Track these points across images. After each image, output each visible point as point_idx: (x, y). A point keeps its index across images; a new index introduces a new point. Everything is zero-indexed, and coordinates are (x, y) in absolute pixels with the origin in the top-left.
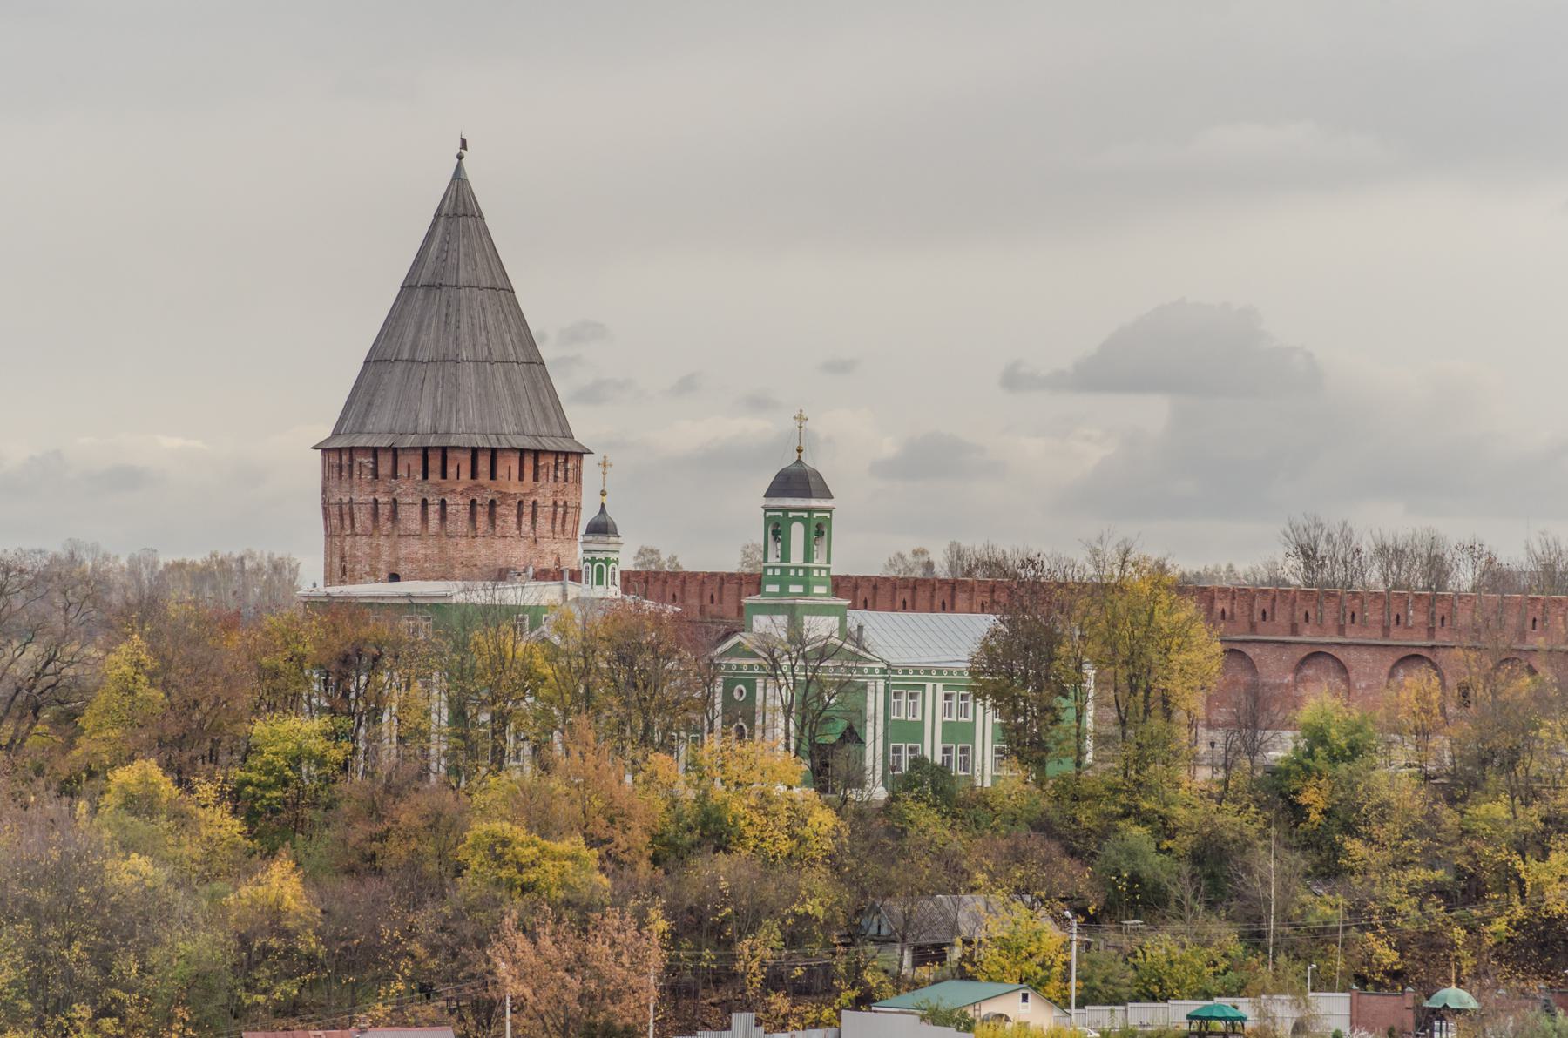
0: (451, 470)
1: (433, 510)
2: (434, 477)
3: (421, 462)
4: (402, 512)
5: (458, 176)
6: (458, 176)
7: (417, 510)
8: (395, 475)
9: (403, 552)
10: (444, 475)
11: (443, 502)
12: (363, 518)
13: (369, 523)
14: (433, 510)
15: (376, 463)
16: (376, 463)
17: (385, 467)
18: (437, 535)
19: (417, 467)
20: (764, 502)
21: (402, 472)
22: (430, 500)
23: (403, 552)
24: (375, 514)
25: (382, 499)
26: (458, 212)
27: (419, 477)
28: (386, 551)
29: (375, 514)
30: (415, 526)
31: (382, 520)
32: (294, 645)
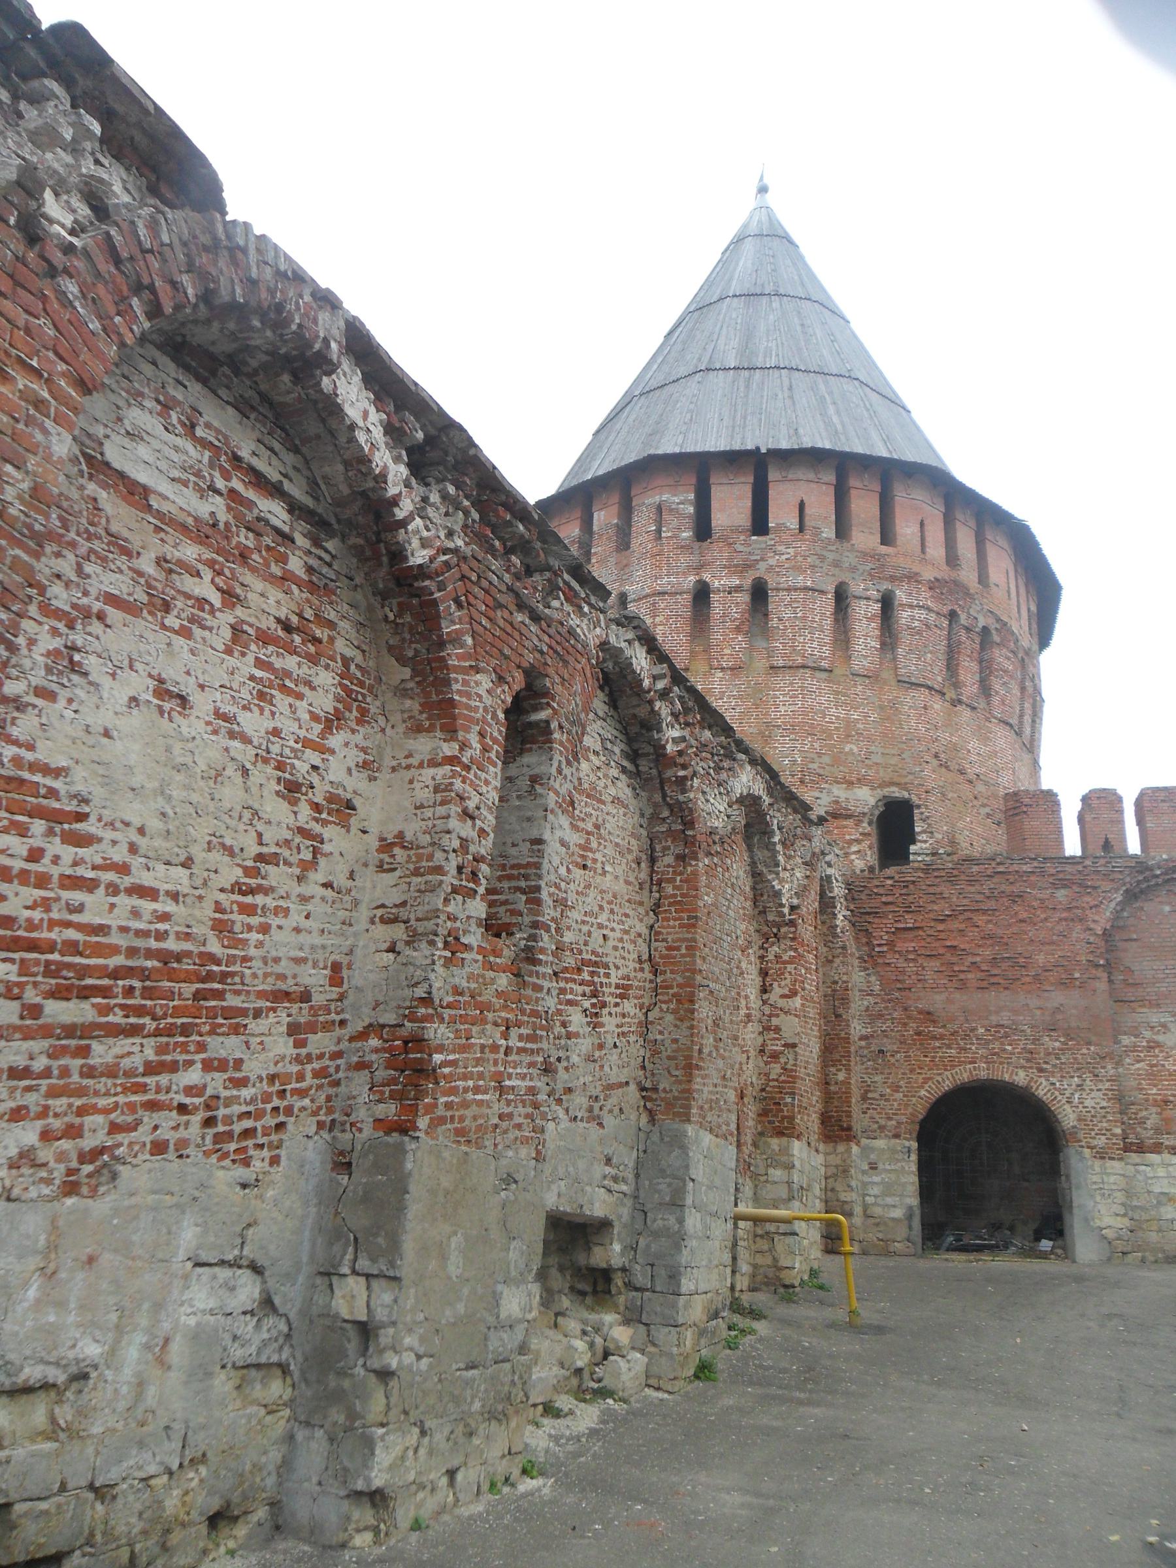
0: (906, 530)
1: (865, 613)
2: (865, 537)
4: (781, 608)
8: (760, 525)
10: (887, 537)
11: (887, 602)
14: (865, 613)
17: (731, 504)
18: (871, 677)
19: (821, 506)
21: (781, 514)
22: (857, 587)
25: (718, 581)
27: (829, 532)
30: (817, 644)
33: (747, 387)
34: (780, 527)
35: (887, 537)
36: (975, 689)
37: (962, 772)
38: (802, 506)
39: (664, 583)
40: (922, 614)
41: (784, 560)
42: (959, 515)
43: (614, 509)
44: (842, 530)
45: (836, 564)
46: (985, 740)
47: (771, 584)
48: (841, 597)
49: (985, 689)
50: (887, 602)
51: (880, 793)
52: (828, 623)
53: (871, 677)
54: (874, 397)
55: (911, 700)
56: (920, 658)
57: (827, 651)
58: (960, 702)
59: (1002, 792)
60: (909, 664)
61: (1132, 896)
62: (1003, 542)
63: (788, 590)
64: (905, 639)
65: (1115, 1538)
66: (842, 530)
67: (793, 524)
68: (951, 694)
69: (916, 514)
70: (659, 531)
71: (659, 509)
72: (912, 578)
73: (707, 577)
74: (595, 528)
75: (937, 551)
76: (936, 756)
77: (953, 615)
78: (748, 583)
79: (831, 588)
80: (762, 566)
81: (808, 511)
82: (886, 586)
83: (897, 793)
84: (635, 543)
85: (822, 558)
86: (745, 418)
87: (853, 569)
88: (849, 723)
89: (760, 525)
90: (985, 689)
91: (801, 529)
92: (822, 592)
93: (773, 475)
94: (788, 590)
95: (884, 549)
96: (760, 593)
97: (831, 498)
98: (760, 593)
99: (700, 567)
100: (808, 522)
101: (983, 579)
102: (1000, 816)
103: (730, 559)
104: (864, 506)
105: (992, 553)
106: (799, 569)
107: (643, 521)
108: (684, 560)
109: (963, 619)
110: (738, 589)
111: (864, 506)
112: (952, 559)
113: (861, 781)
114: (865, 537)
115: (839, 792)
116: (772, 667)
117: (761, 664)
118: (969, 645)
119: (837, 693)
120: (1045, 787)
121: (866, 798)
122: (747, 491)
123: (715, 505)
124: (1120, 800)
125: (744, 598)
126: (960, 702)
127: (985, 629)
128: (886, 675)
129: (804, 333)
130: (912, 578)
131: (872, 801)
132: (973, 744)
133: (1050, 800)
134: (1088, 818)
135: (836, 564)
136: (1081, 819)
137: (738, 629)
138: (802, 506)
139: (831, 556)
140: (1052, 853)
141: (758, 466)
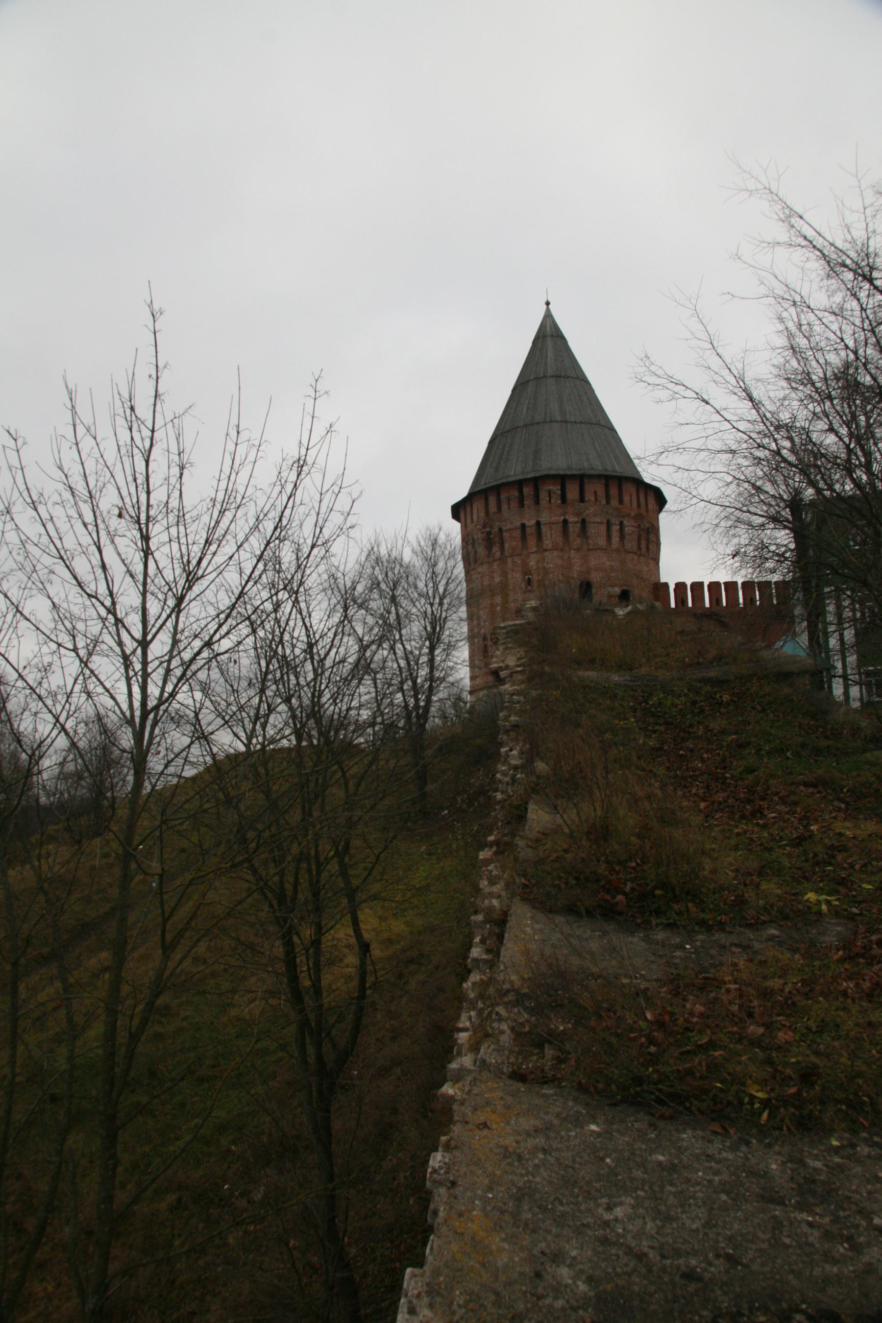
0: (626, 499)
1: (615, 528)
2: (614, 503)
3: (604, 489)
4: (592, 530)
5: (548, 316)
6: (548, 316)
7: (603, 528)
8: (582, 499)
9: (593, 563)
10: (621, 502)
11: (621, 524)
12: (551, 537)
13: (560, 540)
14: (615, 528)
15: (563, 490)
16: (563, 490)
17: (573, 492)
18: (617, 550)
19: (601, 493)
20: (722, 581)
21: (589, 496)
22: (613, 521)
23: (593, 563)
24: (524, 537)
25: (571, 519)
26: (549, 342)
27: (604, 502)
28: (577, 562)
29: (524, 537)
30: (602, 541)
31: (572, 537)
32: (274, 687)
34: (589, 501)
35: (621, 502)
38: (595, 492)
39: (553, 519)
40: (632, 529)
41: (590, 510)
48: (609, 525)
49: (648, 548)
52: (605, 534)
56: (631, 545)
64: (627, 537)
65: (226, 1187)
66: (608, 498)
67: (593, 499)
72: (628, 515)
73: (567, 517)
75: (635, 505)
77: (639, 526)
78: (580, 520)
79: (605, 522)
80: (585, 514)
82: (621, 519)
83: (625, 588)
84: (542, 503)
88: (612, 567)
89: (582, 499)
90: (648, 548)
93: (586, 481)
95: (620, 506)
96: (583, 522)
98: (583, 522)
99: (565, 513)
101: (647, 511)
104: (614, 492)
105: (649, 498)
106: (595, 516)
107: (543, 495)
109: (642, 527)
110: (577, 522)
111: (614, 492)
112: (639, 506)
113: (616, 585)
114: (614, 503)
120: (663, 580)
125: (579, 525)
130: (628, 515)
132: (645, 569)
133: (666, 585)
135: (607, 513)
136: (675, 590)
137: (578, 536)
138: (595, 492)
141: (582, 479)
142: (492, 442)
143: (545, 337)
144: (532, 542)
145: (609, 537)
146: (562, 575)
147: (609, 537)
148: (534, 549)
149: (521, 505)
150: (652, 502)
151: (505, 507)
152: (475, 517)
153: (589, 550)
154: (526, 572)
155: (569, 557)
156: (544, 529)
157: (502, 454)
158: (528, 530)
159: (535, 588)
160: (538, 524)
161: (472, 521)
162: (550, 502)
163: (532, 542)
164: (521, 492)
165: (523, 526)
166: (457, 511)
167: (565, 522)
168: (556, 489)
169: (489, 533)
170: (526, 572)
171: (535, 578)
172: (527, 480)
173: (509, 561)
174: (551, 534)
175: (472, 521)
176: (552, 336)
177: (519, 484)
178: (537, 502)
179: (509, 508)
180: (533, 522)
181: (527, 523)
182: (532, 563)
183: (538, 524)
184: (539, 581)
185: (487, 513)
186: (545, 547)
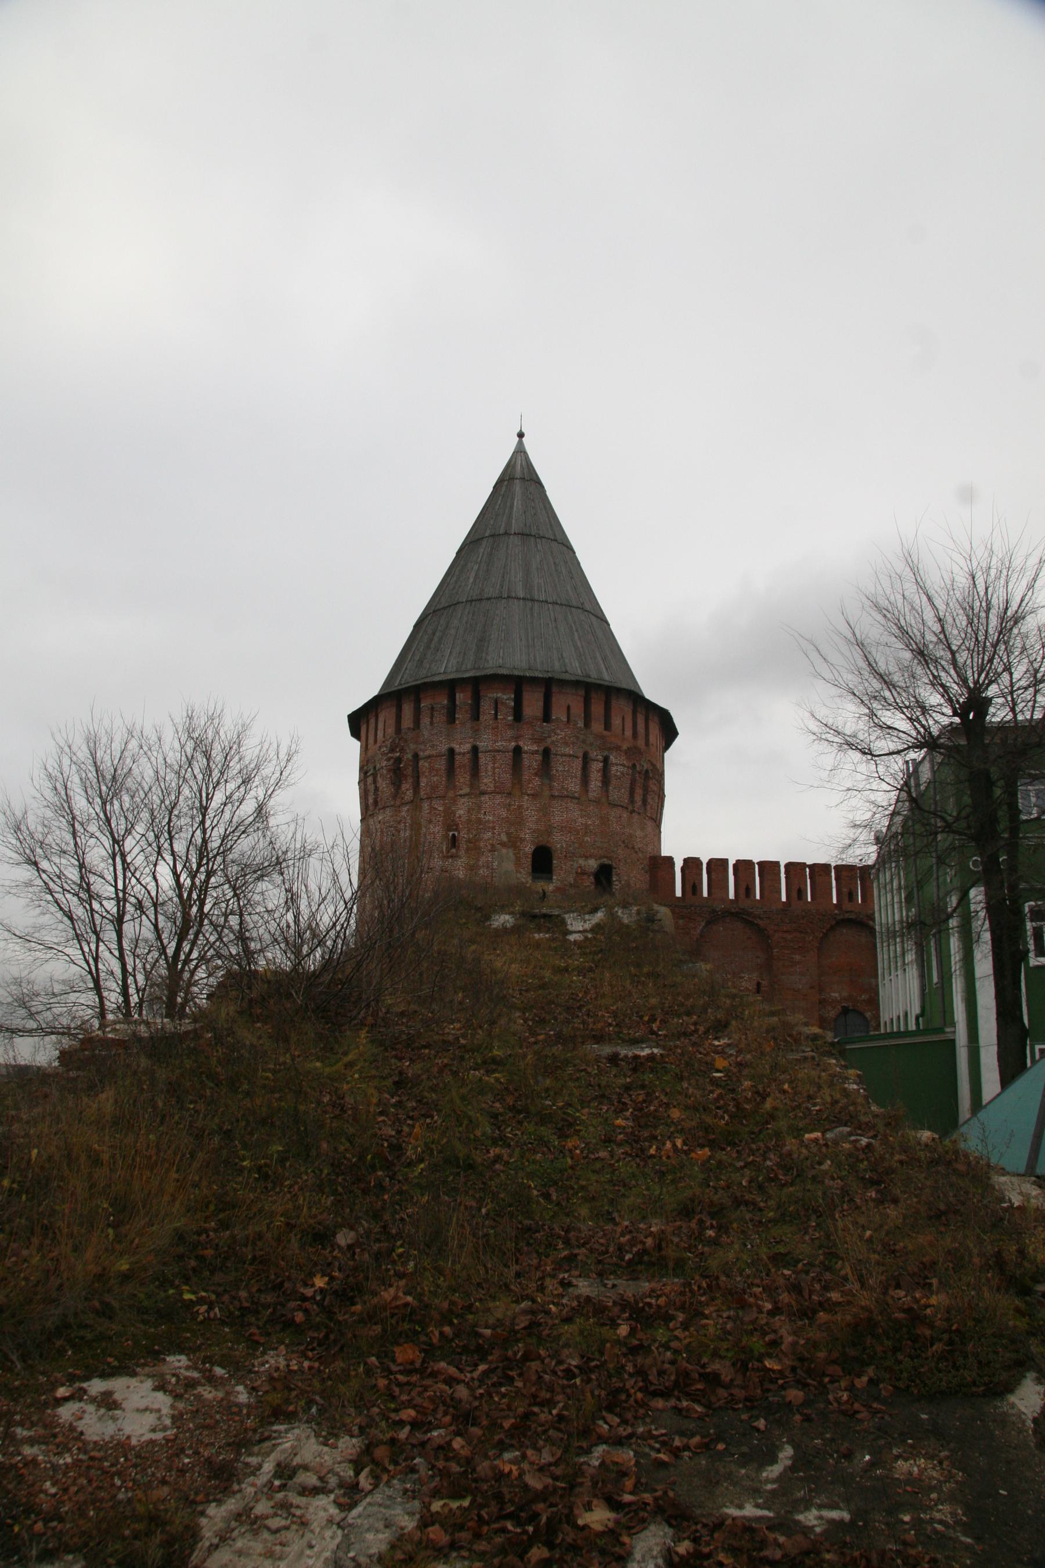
0: (616, 721)
1: (596, 766)
2: (597, 727)
4: (558, 766)
6: (520, 451)
7: (578, 764)
8: (547, 717)
10: (607, 726)
11: (606, 760)
12: (494, 771)
13: (507, 777)
14: (596, 766)
17: (533, 705)
18: (597, 802)
19: (578, 710)
21: (558, 713)
22: (593, 754)
23: (558, 817)
25: (527, 747)
27: (581, 724)
30: (574, 786)
33: (532, 615)
34: (557, 719)
35: (607, 726)
36: (640, 803)
37: (633, 848)
38: (569, 708)
42: (639, 709)
43: (469, 694)
44: (587, 724)
45: (584, 742)
46: (643, 829)
47: (553, 750)
49: (645, 802)
50: (606, 760)
51: (599, 862)
53: (597, 802)
54: (593, 619)
55: (614, 813)
56: (618, 793)
57: (578, 788)
58: (634, 811)
59: (648, 855)
60: (614, 795)
61: (708, 923)
62: (656, 719)
63: (562, 755)
64: (614, 782)
66: (587, 724)
68: (630, 808)
69: (621, 709)
70: (496, 714)
71: (496, 702)
72: (618, 748)
73: (521, 744)
74: (457, 703)
75: (628, 733)
76: (624, 842)
77: (634, 765)
78: (542, 748)
79: (581, 755)
80: (549, 740)
81: (572, 712)
82: (606, 753)
83: (606, 861)
85: (577, 738)
86: (533, 640)
87: (591, 744)
88: (587, 826)
89: (547, 717)
90: (645, 802)
91: (568, 721)
92: (577, 757)
93: (554, 689)
94: (562, 755)
95: (606, 733)
96: (546, 753)
97: (582, 705)
98: (546, 753)
99: (517, 738)
100: (572, 718)
101: (647, 744)
102: (647, 868)
103: (533, 735)
106: (566, 744)
107: (486, 706)
108: (510, 733)
109: (638, 768)
110: (536, 752)
112: (635, 735)
113: (591, 856)
114: (597, 727)
115: (582, 862)
116: (552, 796)
117: (547, 793)
118: (640, 781)
119: (581, 810)
121: (593, 864)
122: (541, 696)
123: (525, 703)
124: (702, 864)
125: (539, 757)
126: (634, 811)
127: (647, 771)
128: (604, 800)
129: (556, 571)
130: (618, 748)
131: (595, 866)
134: (687, 872)
135: (584, 742)
136: (683, 869)
137: (536, 774)
138: (569, 708)
139: (582, 737)
140: (572, 665)
141: (549, 685)
142: (418, 626)
143: (512, 479)
144: (463, 778)
145: (585, 780)
146: (508, 834)
147: (585, 780)
148: (466, 790)
149: (451, 719)
150: (655, 731)
151: (425, 721)
152: (380, 734)
153: (553, 796)
154: (451, 825)
155: (520, 807)
156: (483, 759)
157: (431, 640)
158: (457, 757)
159: (462, 853)
160: (475, 750)
161: (376, 742)
162: (496, 718)
163: (463, 778)
164: (452, 699)
165: (451, 752)
166: (358, 722)
167: (518, 751)
168: (507, 697)
169: (398, 760)
170: (451, 825)
171: (463, 835)
172: (534, 681)
173: (426, 805)
174: (494, 768)
175: (376, 742)
176: (523, 479)
177: (451, 686)
178: (476, 717)
179: (432, 723)
180: (467, 747)
181: (457, 748)
182: (461, 812)
183: (475, 750)
184: (469, 841)
185: (398, 729)
186: (483, 788)
